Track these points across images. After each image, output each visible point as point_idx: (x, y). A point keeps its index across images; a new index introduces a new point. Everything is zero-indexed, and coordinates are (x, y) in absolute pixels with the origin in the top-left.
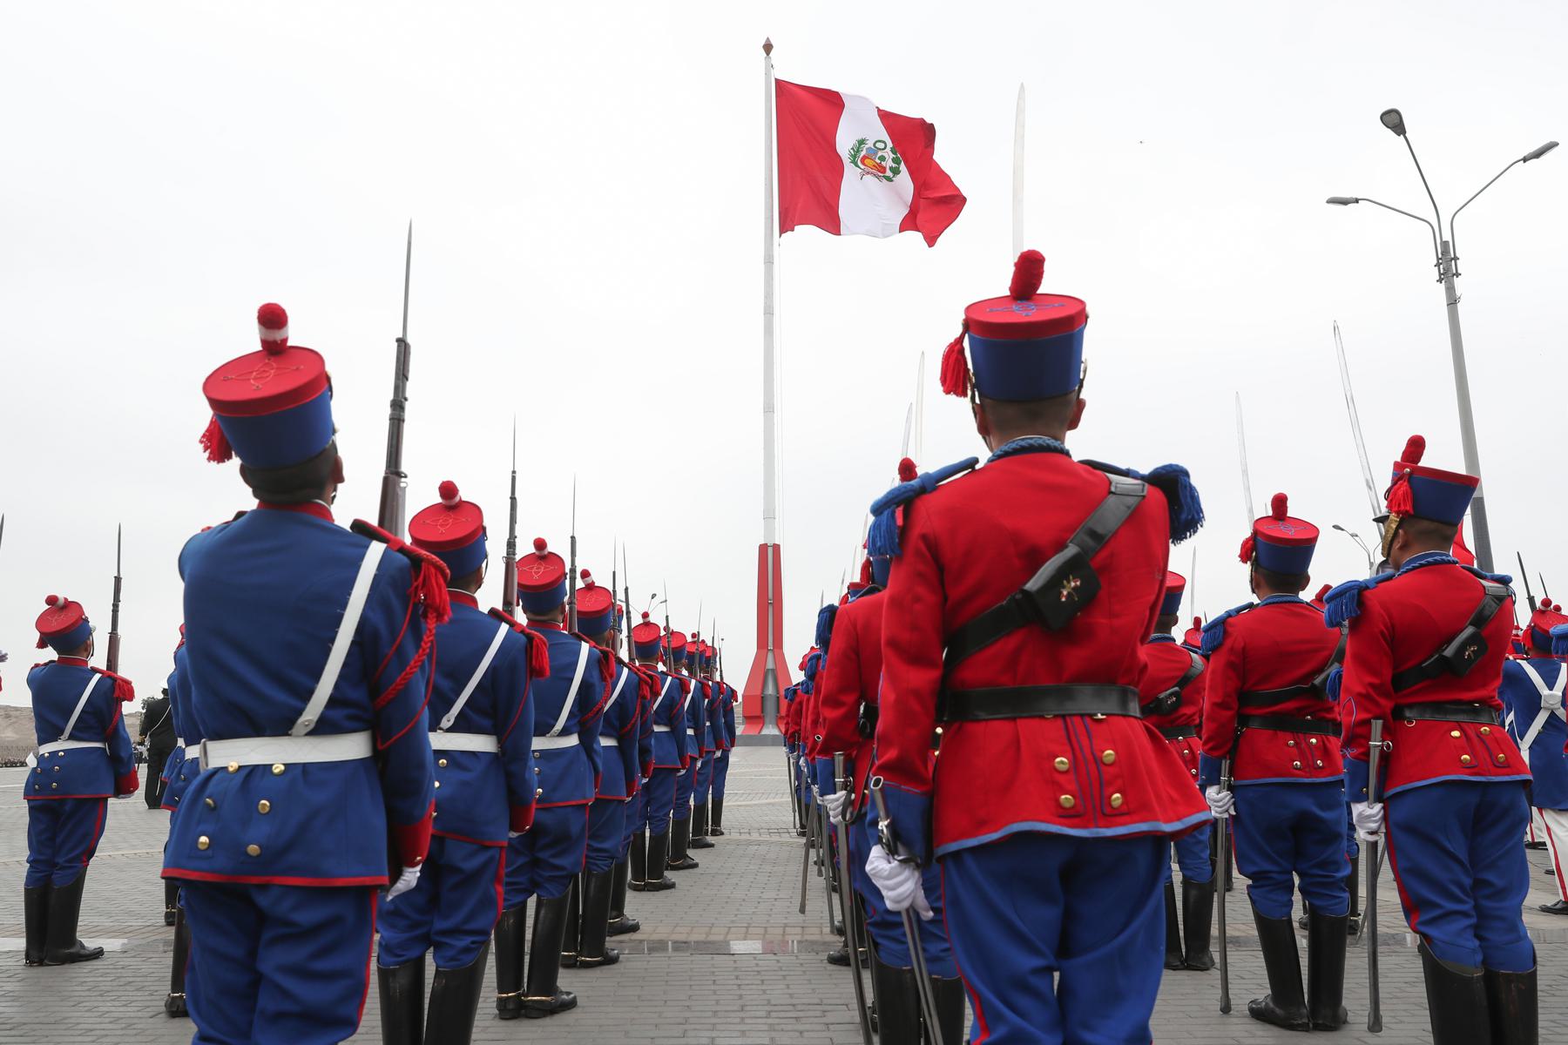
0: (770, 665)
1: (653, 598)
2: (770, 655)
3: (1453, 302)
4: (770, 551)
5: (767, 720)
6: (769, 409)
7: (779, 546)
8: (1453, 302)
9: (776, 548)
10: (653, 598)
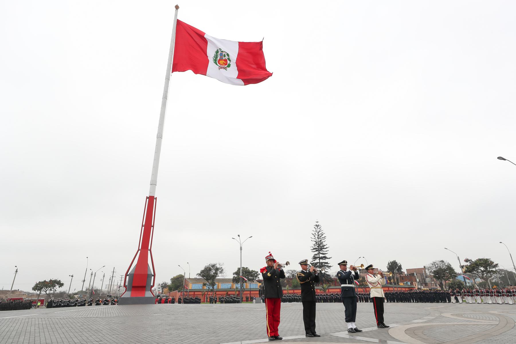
3: (241, 252)
6: (160, 136)
8: (241, 252)
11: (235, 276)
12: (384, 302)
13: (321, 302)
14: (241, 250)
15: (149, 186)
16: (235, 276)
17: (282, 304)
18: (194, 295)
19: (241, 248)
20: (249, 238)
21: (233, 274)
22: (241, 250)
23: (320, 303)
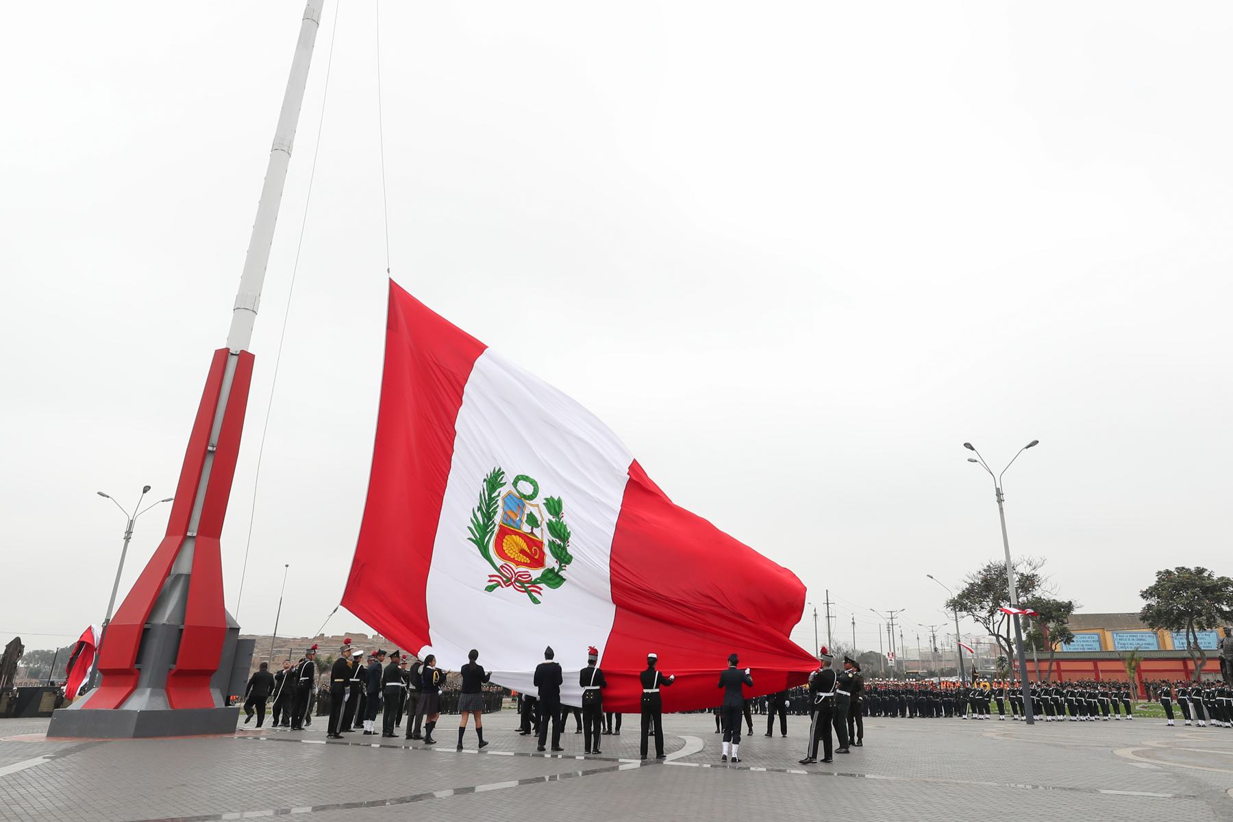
0: (185, 565)
1: (145, 491)
2: (189, 551)
3: (1001, 509)
4: (232, 363)
5: (146, 677)
6: (282, 147)
7: (252, 357)
8: (1001, 509)
9: (246, 360)
10: (145, 491)
11: (1153, 601)
12: (563, 732)
13: (938, 715)
14: (1000, 501)
15: (229, 316)
16: (1153, 601)
17: (662, 715)
18: (1096, 671)
19: (999, 493)
20: (1027, 447)
21: (1144, 597)
22: (1000, 501)
23: (899, 719)
